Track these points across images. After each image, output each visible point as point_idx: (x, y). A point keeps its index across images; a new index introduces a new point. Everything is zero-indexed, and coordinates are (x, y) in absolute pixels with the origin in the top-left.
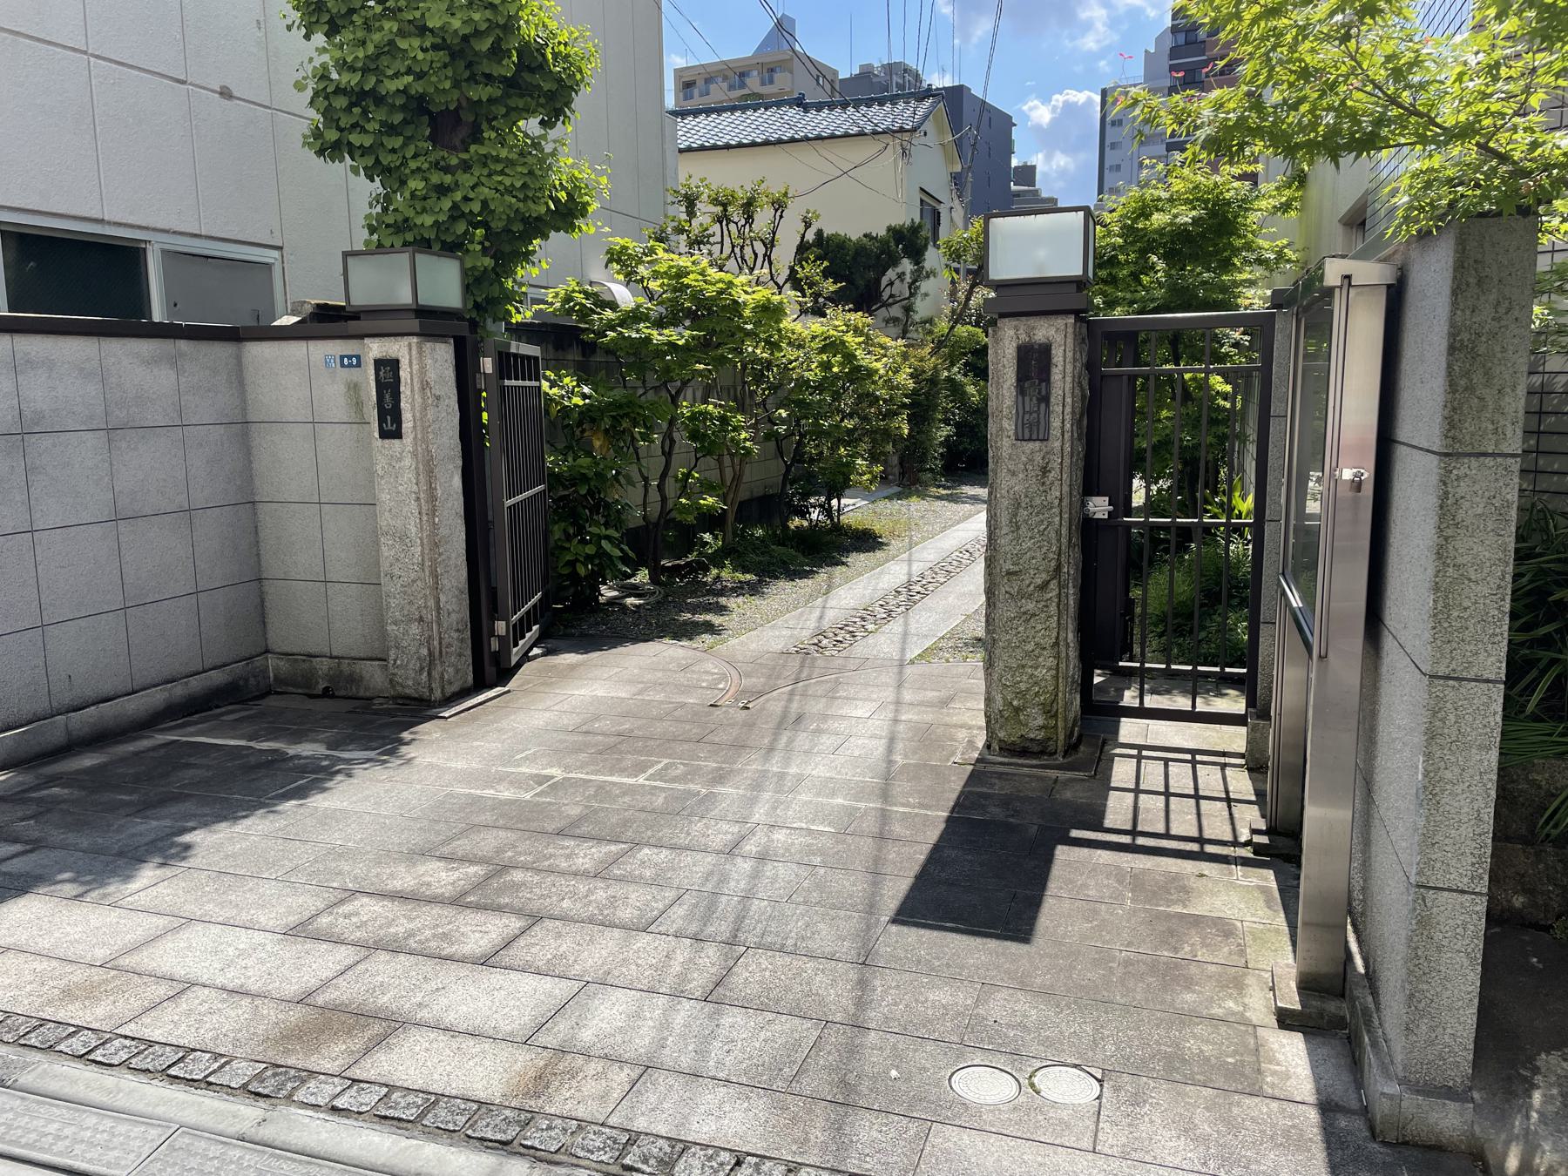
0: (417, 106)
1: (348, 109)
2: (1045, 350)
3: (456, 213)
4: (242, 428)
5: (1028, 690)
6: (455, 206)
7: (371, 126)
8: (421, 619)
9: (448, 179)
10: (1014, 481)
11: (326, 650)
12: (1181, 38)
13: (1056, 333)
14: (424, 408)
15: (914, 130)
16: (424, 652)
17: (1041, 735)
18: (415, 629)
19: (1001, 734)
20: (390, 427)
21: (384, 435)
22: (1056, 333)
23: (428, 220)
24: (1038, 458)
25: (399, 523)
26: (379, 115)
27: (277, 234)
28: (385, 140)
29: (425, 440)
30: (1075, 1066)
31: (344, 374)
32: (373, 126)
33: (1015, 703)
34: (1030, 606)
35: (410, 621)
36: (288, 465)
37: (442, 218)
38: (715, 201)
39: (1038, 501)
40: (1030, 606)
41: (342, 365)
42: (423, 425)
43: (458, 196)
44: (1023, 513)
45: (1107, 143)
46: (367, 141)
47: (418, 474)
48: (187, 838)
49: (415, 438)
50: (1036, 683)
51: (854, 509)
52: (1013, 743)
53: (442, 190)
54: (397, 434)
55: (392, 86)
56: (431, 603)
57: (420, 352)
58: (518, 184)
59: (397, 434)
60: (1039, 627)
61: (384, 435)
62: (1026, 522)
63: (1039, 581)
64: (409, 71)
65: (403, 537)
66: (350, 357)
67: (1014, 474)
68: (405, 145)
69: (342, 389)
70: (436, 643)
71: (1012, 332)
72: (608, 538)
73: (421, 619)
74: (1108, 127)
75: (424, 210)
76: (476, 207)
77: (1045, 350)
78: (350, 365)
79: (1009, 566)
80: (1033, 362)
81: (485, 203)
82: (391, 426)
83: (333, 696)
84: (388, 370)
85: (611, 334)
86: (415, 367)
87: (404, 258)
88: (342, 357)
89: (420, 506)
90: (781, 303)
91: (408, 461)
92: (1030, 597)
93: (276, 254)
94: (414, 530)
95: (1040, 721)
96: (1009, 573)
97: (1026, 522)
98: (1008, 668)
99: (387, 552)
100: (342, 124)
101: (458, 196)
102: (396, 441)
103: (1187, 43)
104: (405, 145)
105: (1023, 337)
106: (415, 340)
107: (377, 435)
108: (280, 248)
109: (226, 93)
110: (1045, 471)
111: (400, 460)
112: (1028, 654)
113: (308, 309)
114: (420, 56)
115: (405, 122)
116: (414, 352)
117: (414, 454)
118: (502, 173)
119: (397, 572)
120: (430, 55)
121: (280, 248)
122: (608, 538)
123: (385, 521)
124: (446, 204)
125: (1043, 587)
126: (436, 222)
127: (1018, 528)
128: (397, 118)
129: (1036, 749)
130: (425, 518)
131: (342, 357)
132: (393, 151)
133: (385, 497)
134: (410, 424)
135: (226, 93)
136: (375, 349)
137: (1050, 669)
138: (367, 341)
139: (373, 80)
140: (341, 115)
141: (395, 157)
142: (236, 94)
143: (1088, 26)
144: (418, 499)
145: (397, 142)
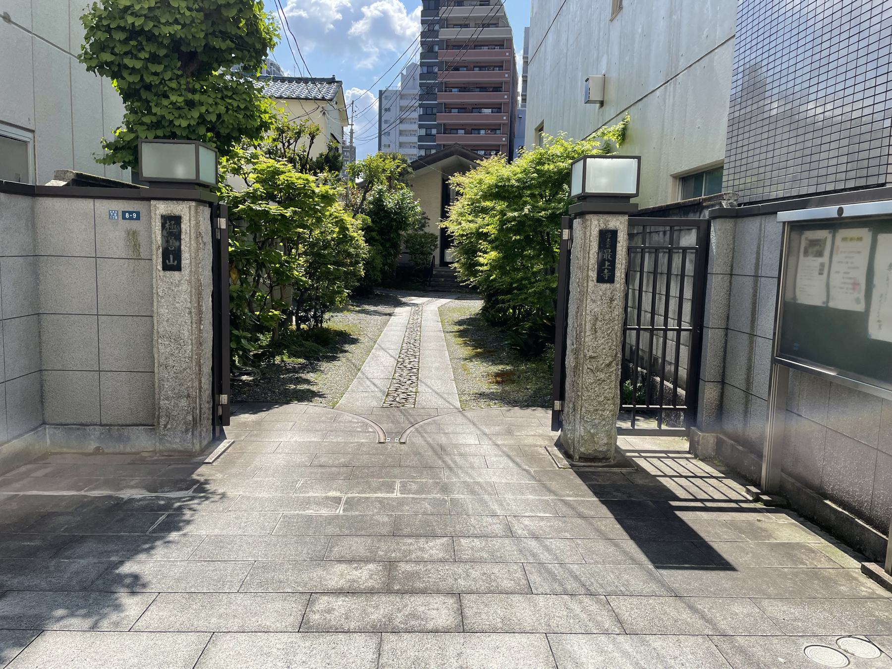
0: (176, 44)
1: (126, 41)
2: (614, 233)
3: (202, 120)
4: (34, 258)
5: (599, 423)
6: (201, 116)
7: (143, 55)
8: (188, 396)
9: (197, 97)
10: (594, 305)
11: (97, 420)
12: (425, 69)
13: (619, 223)
14: (198, 249)
15: (331, 100)
16: (190, 418)
17: (604, 449)
18: (184, 403)
19: (582, 449)
20: (171, 262)
21: (166, 268)
22: (619, 223)
23: (184, 124)
24: (609, 293)
25: (174, 330)
26: (150, 48)
27: (32, 121)
28: (149, 65)
29: (196, 272)
30: (850, 636)
31: (127, 224)
32: (143, 55)
33: (592, 431)
34: (602, 376)
35: (180, 397)
36: (72, 287)
37: (193, 123)
38: (278, 129)
39: (607, 317)
40: (602, 376)
41: (124, 218)
42: (196, 261)
43: (203, 109)
44: (599, 324)
45: (383, 119)
46: (138, 65)
47: (191, 296)
48: (128, 568)
49: (191, 271)
50: (604, 419)
51: (335, 321)
52: (590, 454)
53: (191, 104)
54: (178, 268)
55: (167, 30)
56: (196, 384)
57: (196, 212)
58: (242, 106)
59: (178, 268)
60: (606, 387)
61: (166, 268)
62: (600, 328)
63: (607, 362)
64: (176, 22)
65: (177, 339)
66: (131, 213)
67: (594, 301)
68: (165, 71)
69: (123, 235)
70: (198, 411)
71: (596, 222)
72: (245, 338)
73: (188, 396)
74: (383, 111)
75: (180, 117)
76: (213, 118)
77: (614, 233)
78: (131, 218)
79: (590, 354)
80: (608, 239)
81: (219, 116)
82: (172, 260)
83: (103, 453)
84: (172, 224)
85: (241, 206)
86: (193, 223)
87: (192, 147)
88: (124, 213)
89: (191, 317)
90: (334, 194)
91: (185, 287)
92: (602, 371)
93: (30, 135)
94: (186, 333)
95: (605, 441)
96: (591, 357)
97: (600, 328)
98: (588, 412)
99: (163, 348)
100: (116, 50)
101: (203, 109)
102: (176, 273)
103: (428, 73)
104: (165, 71)
105: (603, 226)
106: (194, 204)
107: (160, 267)
108: (33, 131)
109: (7, 18)
110: (612, 300)
111: (177, 286)
112: (600, 403)
113: (71, 176)
114: (188, 13)
115: (166, 56)
116: (193, 212)
117: (189, 282)
118: (231, 98)
119: (171, 363)
120: (194, 14)
121: (33, 131)
122: (245, 338)
123: (162, 327)
124: (196, 114)
125: (609, 365)
126: (189, 125)
127: (596, 332)
128: (162, 52)
129: (601, 457)
130: (194, 326)
131: (124, 213)
132: (156, 74)
133: (164, 311)
134: (188, 262)
135: (7, 18)
136: (162, 208)
137: (611, 411)
138: (153, 202)
139: (151, 24)
140: (118, 45)
141: (156, 78)
142: (13, 19)
143: (368, 55)
144: (190, 313)
145: (159, 68)
